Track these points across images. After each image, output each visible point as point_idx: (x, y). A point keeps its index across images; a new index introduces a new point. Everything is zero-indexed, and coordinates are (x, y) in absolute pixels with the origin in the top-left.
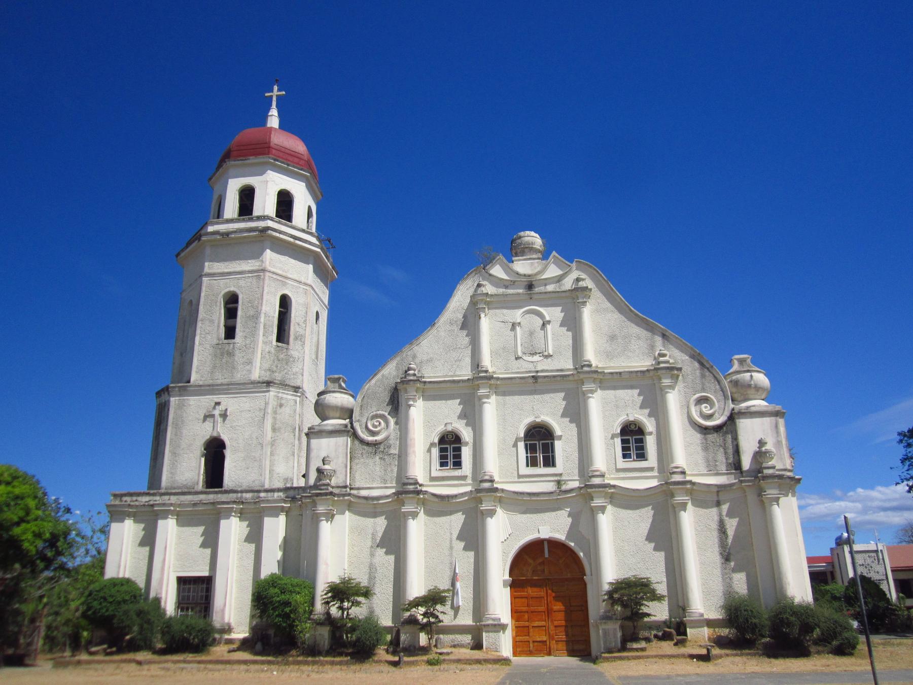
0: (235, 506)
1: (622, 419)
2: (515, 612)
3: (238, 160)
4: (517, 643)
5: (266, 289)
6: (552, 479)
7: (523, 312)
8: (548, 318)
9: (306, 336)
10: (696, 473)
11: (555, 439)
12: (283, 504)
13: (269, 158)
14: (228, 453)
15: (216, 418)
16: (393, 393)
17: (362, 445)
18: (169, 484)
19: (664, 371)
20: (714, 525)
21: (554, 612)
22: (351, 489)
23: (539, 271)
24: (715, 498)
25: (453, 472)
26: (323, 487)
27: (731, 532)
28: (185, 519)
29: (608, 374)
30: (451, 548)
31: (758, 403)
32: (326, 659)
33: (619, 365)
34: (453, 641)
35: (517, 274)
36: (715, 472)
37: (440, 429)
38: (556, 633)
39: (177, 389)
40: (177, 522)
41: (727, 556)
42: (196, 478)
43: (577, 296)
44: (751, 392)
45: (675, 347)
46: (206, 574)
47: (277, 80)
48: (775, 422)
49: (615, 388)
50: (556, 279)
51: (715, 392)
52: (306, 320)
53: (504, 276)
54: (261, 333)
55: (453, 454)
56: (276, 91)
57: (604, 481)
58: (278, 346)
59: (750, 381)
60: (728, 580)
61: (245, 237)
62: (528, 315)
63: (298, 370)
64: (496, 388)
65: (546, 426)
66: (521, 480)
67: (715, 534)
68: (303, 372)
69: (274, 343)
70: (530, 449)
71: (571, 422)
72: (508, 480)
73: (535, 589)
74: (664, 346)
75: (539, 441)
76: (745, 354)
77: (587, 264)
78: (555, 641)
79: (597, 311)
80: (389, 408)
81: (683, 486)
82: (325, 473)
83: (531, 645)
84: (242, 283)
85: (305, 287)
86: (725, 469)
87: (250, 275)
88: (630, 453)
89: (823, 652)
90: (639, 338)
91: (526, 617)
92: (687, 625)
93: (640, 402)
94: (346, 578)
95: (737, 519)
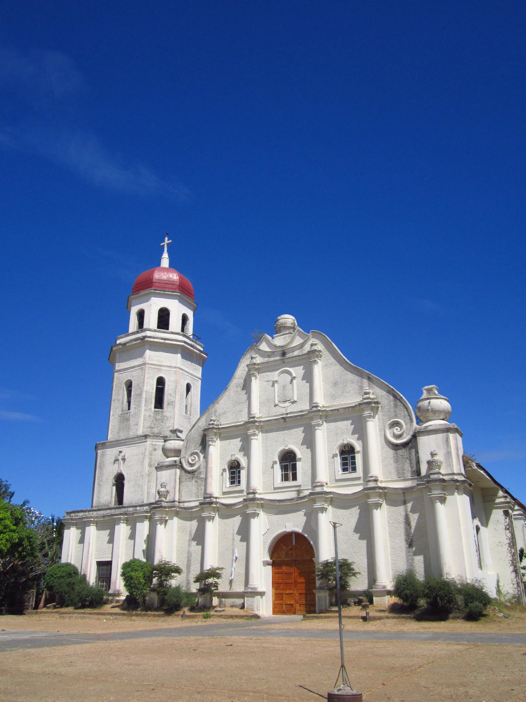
0: (122, 516)
1: (340, 442)
2: (275, 584)
3: (135, 295)
4: (276, 605)
5: (147, 376)
6: (294, 489)
7: (279, 373)
8: (294, 375)
9: (176, 402)
10: (389, 480)
11: (297, 460)
12: (145, 514)
13: (151, 290)
14: (126, 482)
15: (120, 461)
16: (203, 437)
17: (186, 473)
18: (97, 504)
19: (364, 406)
20: (402, 519)
21: (299, 583)
22: (179, 502)
23: (289, 343)
24: (403, 499)
25: (235, 488)
26: (159, 503)
27: (413, 524)
28: (100, 526)
29: (330, 411)
30: (233, 539)
31: (437, 423)
32: (152, 613)
33: (340, 404)
34: (233, 602)
35: (275, 346)
36: (403, 478)
37: (229, 458)
38: (300, 599)
39: (100, 445)
40: (96, 527)
41: (410, 542)
42: (110, 499)
43: (313, 354)
44: (430, 414)
45: (377, 386)
46: (110, 560)
47: (167, 234)
48: (446, 437)
49: (336, 421)
50: (300, 346)
51: (404, 417)
52: (176, 391)
53: (267, 349)
54: (143, 405)
55: (351, 462)
56: (167, 241)
57: (377, 484)
58: (155, 411)
59: (428, 406)
60: (410, 561)
61: (134, 344)
62: (284, 374)
63: (170, 424)
64: (261, 428)
65: (285, 452)
66: (276, 491)
67: (402, 526)
68: (174, 426)
69: (153, 409)
70: (284, 468)
71: (307, 448)
72: (268, 492)
73: (288, 568)
74: (369, 386)
75: (290, 462)
76: (433, 385)
77: (319, 333)
78: (298, 605)
79: (325, 366)
80: (200, 448)
81: (374, 491)
82: (160, 493)
83: (284, 607)
84: (134, 373)
85: (175, 370)
86: (410, 476)
87: (138, 368)
88: (348, 468)
89: (458, 618)
90: (353, 382)
91: (282, 587)
92: (374, 595)
93: (352, 429)
94: (163, 562)
95: (418, 514)
